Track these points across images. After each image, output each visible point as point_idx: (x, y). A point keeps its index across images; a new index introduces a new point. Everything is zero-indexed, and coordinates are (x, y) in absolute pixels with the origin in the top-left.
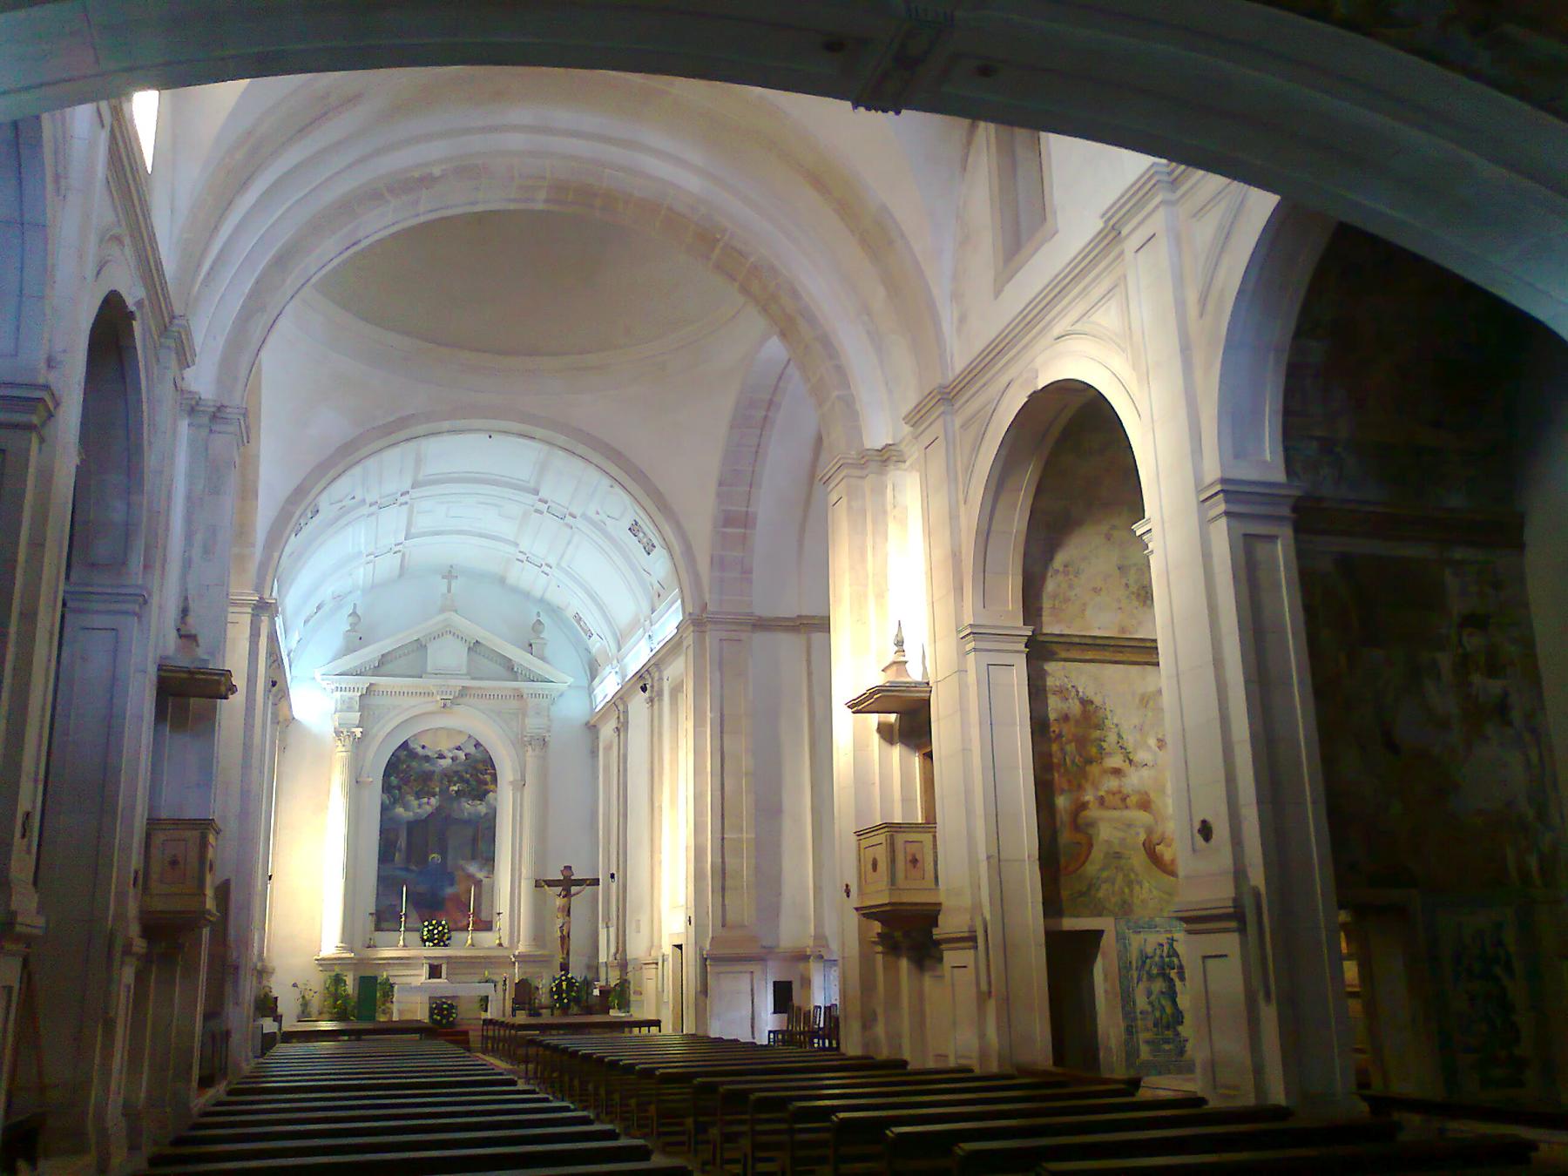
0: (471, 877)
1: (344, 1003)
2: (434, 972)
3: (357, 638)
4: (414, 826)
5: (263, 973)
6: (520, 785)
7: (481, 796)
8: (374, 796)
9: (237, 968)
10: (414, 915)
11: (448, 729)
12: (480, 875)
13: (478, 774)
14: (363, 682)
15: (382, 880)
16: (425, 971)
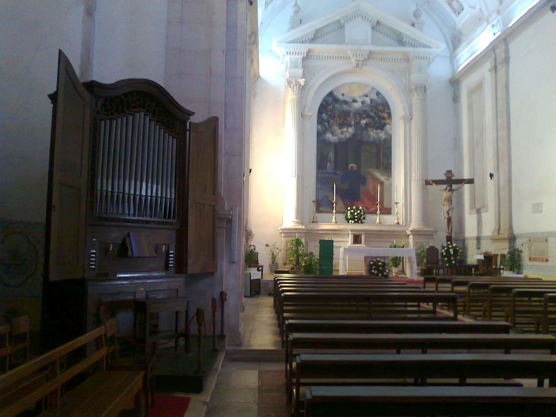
0: (377, 180)
1: (310, 260)
2: (357, 239)
3: (298, 20)
4: (340, 146)
5: (249, 235)
6: (408, 119)
7: (382, 127)
8: (313, 127)
9: (230, 221)
10: (341, 204)
11: (361, 83)
12: (382, 178)
13: (379, 112)
14: (304, 48)
15: (319, 180)
16: (350, 239)
